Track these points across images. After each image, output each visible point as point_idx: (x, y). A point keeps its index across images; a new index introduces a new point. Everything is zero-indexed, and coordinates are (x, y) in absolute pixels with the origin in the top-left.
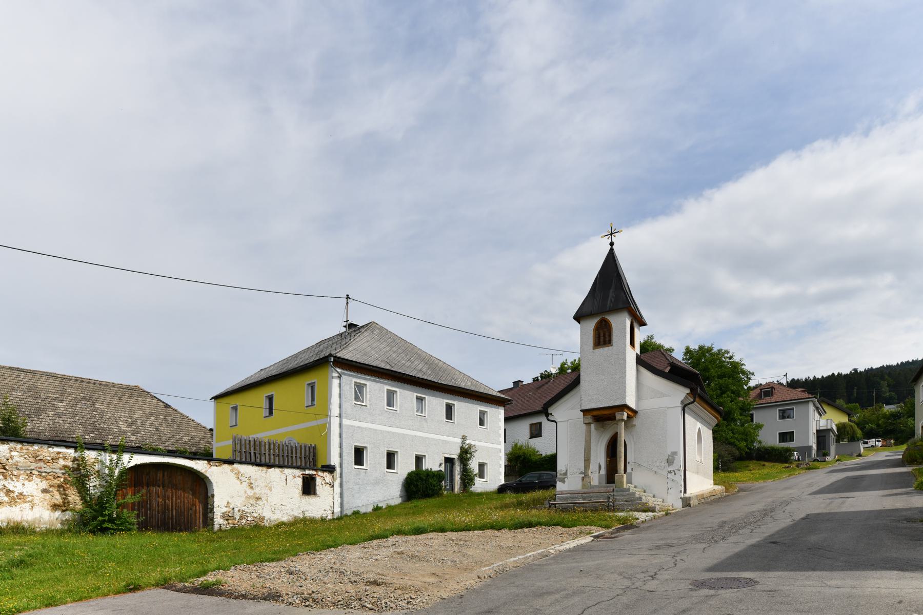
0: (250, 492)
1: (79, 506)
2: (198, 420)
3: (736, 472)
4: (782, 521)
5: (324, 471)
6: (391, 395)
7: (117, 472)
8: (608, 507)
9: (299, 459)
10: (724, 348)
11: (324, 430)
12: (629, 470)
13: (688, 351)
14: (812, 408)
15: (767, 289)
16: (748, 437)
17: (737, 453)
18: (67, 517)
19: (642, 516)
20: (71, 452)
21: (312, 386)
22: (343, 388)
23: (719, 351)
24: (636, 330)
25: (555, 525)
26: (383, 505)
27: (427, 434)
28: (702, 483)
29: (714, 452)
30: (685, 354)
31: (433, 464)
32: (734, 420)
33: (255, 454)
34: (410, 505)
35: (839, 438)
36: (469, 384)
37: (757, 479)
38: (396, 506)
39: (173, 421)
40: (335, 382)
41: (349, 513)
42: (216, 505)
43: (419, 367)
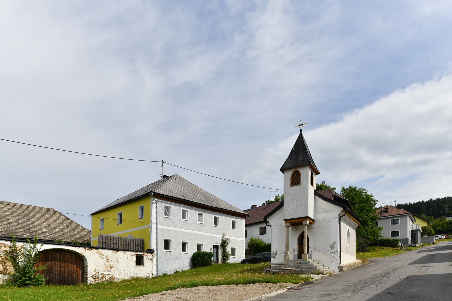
0: (107, 264)
1: (13, 272)
2: (84, 226)
3: (368, 252)
4: (394, 280)
5: (148, 253)
6: (184, 213)
7: (34, 254)
8: (298, 272)
9: (134, 247)
10: (362, 188)
11: (148, 230)
12: (310, 252)
13: (343, 189)
14: (408, 219)
15: (387, 160)
16: (375, 234)
17: (369, 242)
18: (6, 278)
19: (316, 277)
20: (8, 243)
21: (142, 208)
22: (158, 209)
23: (360, 189)
24: (314, 176)
25: (268, 282)
26: (180, 270)
27: (204, 233)
28: (349, 258)
29: (356, 242)
30: (342, 191)
31: (207, 249)
32: (368, 225)
33: (111, 244)
34: (194, 270)
35: (423, 234)
36: (227, 206)
37: (379, 256)
38: (186, 271)
40: (154, 206)
41: (161, 274)
42: (88, 271)
43: (200, 198)
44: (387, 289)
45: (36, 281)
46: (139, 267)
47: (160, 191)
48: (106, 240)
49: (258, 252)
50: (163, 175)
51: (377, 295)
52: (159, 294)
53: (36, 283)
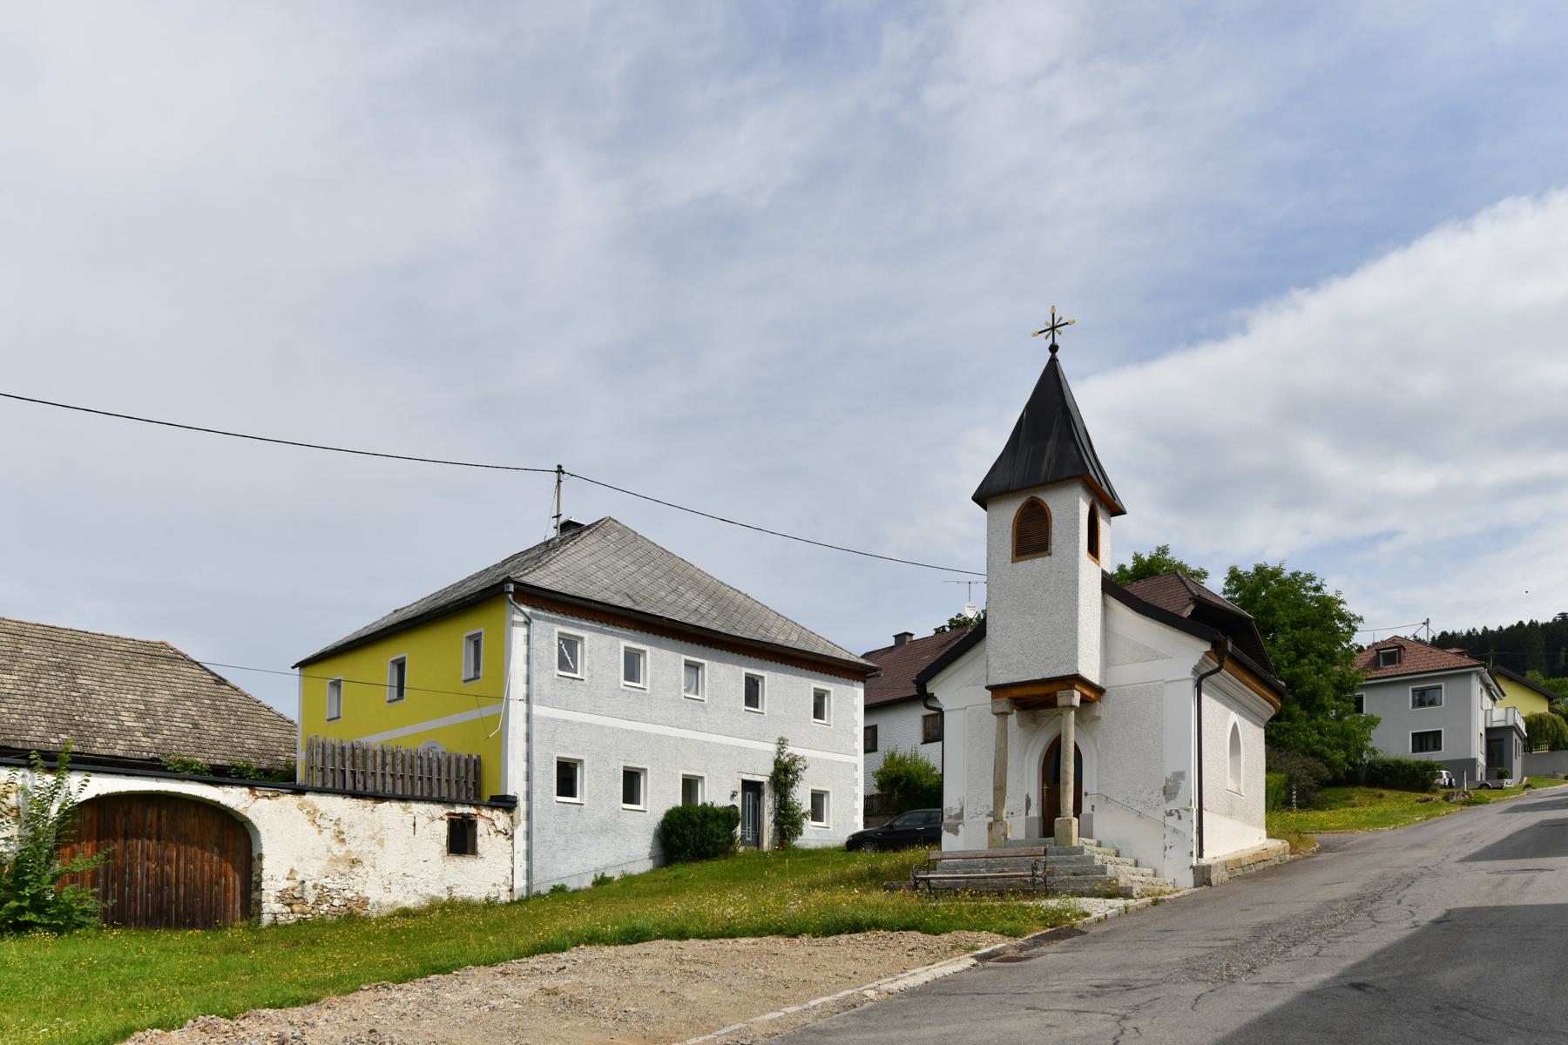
0: (339, 850)
2: (278, 709)
3: (1323, 809)
4: (1393, 927)
5: (493, 808)
7: (54, 809)
8: (1033, 891)
9: (444, 785)
10: (1304, 570)
11: (498, 724)
12: (1086, 809)
13: (1234, 576)
14: (1476, 686)
15: (1410, 478)
16: (1350, 741)
17: (1326, 773)
19: (1098, 907)
21: (476, 641)
23: (1295, 575)
25: (907, 928)
26: (614, 873)
27: (708, 733)
28: (1238, 831)
29: (1269, 770)
30: (1229, 582)
31: (718, 793)
32: (1323, 709)
33: (353, 773)
34: (668, 873)
35: (1530, 743)
36: (794, 637)
38: (641, 877)
39: (229, 708)
40: (519, 633)
41: (545, 889)
42: (266, 874)
43: (694, 605)
44: (1353, 967)
45: (61, 913)
46: (458, 859)
47: (541, 578)
48: (338, 758)
49: (905, 804)
50: (562, 519)
51: (1310, 995)
52: (491, 970)
53: (64, 924)
